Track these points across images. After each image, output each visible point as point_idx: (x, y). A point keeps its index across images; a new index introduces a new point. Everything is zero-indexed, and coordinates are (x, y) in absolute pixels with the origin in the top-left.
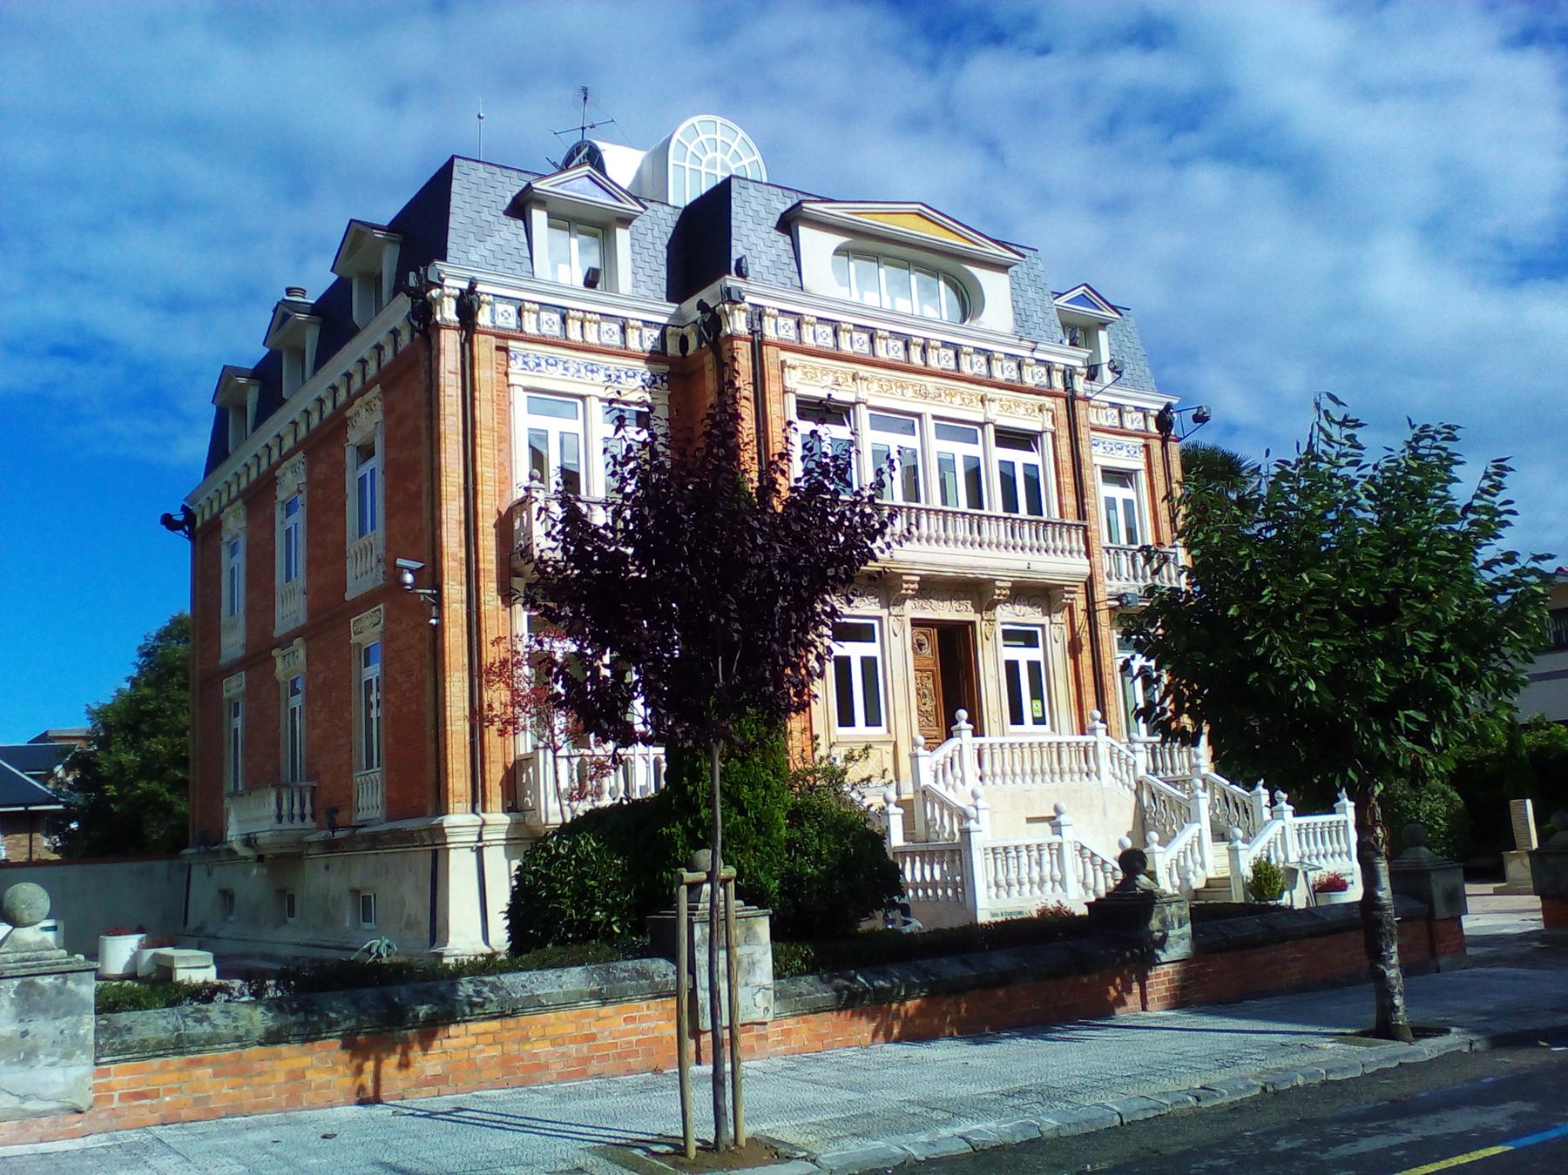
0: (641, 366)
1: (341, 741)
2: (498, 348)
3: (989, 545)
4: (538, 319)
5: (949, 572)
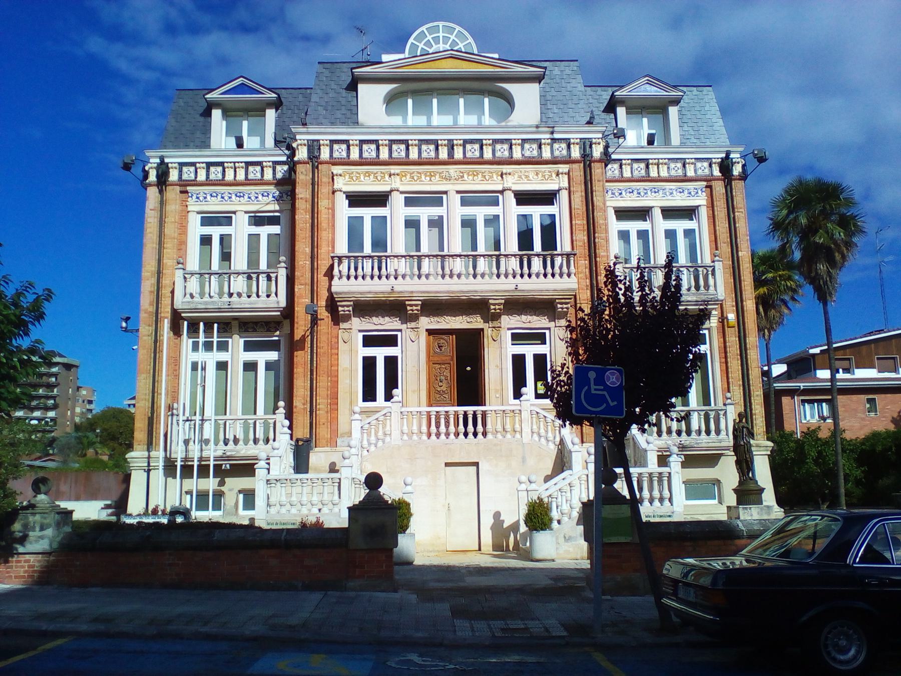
0: (272, 189)
2: (181, 192)
3: (451, 276)
4: (632, 168)
5: (444, 296)
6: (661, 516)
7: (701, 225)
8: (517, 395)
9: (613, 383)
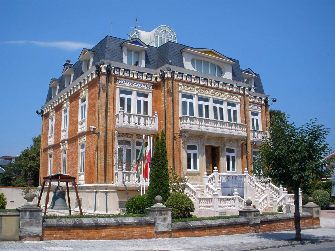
1: (75, 165)
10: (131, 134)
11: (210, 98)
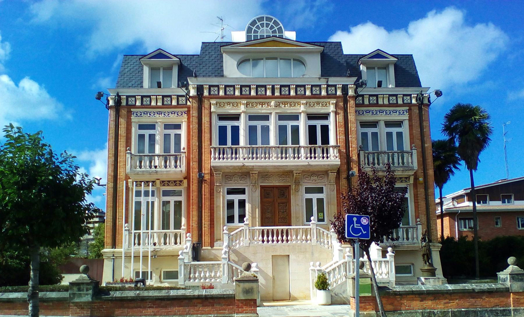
6: (384, 283)
7: (405, 129)
8: (309, 220)
9: (365, 223)
10: (406, 178)
11: (271, 113)
